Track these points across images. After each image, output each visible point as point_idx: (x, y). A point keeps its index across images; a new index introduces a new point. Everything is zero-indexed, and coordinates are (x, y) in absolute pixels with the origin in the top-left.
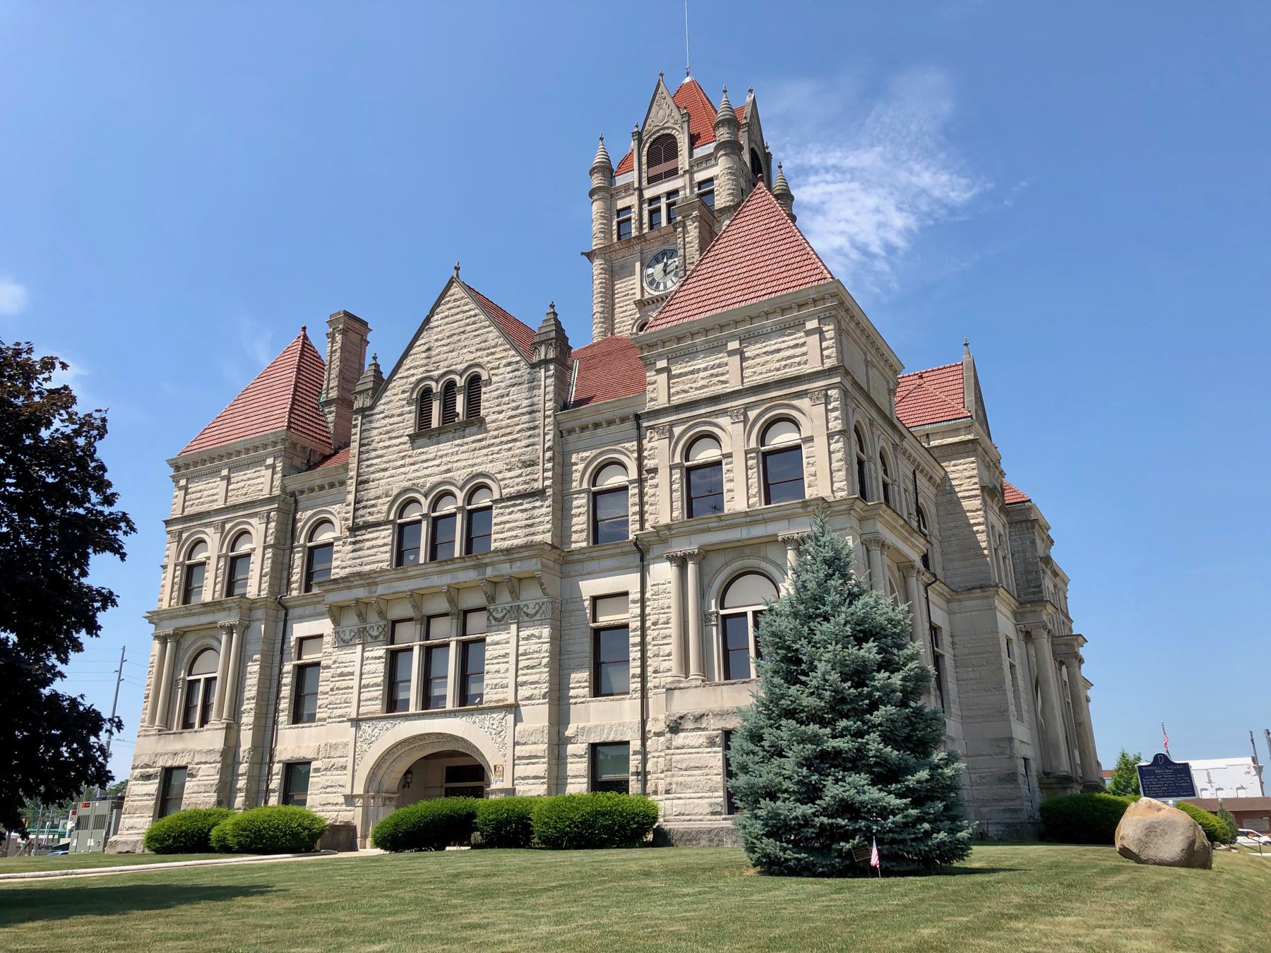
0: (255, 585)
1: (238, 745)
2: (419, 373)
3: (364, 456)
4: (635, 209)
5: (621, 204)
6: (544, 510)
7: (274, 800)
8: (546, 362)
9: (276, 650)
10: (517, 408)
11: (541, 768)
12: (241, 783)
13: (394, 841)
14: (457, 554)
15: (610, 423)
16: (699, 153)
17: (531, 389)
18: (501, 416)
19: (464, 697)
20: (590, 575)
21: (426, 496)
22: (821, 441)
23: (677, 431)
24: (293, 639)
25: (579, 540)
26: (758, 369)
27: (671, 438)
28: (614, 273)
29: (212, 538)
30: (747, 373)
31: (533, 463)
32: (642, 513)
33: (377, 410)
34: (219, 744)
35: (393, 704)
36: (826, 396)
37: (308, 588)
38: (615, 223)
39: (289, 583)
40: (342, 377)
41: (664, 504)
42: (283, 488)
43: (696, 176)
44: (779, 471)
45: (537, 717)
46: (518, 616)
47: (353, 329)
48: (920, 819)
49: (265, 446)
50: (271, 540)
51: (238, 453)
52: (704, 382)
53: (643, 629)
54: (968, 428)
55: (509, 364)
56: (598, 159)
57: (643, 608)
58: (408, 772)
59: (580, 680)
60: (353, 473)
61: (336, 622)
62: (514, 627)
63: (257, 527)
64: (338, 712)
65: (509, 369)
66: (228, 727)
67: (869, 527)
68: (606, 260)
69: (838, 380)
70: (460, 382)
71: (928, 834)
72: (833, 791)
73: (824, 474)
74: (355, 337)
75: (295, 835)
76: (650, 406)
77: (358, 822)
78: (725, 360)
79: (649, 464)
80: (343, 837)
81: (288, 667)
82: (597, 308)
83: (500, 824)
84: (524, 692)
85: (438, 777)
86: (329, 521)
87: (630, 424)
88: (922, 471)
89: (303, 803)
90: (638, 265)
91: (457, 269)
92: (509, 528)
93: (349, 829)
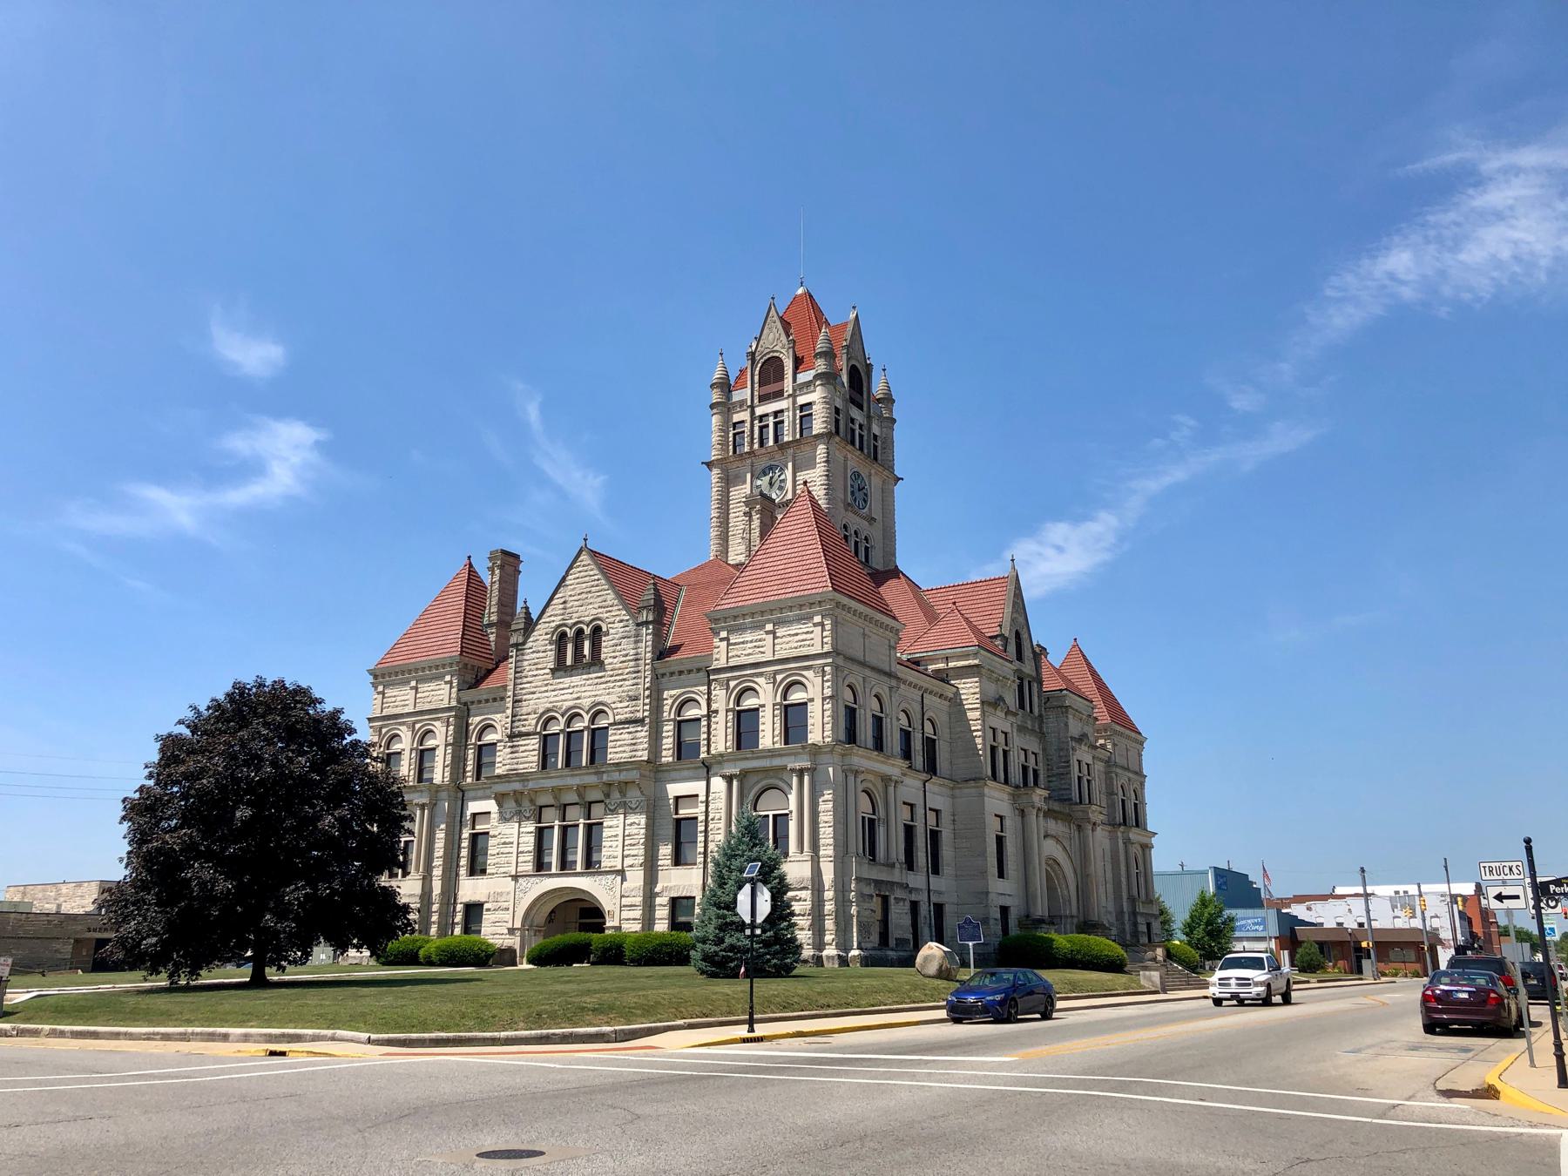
0: (440, 773)
2: (557, 621)
4: (748, 424)
5: (736, 418)
7: (458, 930)
8: (646, 623)
9: (457, 820)
11: (638, 913)
12: (435, 918)
13: (539, 959)
17: (636, 642)
19: (589, 863)
20: (674, 781)
22: (818, 702)
23: (732, 684)
25: (667, 756)
28: (728, 481)
29: (405, 734)
31: (636, 699)
32: (709, 740)
34: (418, 891)
35: (540, 866)
40: (501, 604)
41: (721, 739)
42: (459, 701)
45: (636, 878)
46: (628, 809)
47: (509, 562)
49: (444, 666)
50: (451, 740)
53: (706, 821)
54: (976, 655)
56: (718, 375)
58: (553, 911)
59: (666, 851)
61: (500, 805)
63: (439, 728)
66: (424, 878)
67: (847, 760)
70: (587, 631)
72: (728, 941)
73: (820, 727)
74: (509, 569)
75: (477, 956)
76: (715, 665)
77: (517, 947)
80: (506, 957)
81: (466, 834)
82: (714, 514)
83: (606, 950)
84: (628, 861)
85: (574, 915)
87: (702, 674)
92: (625, 747)
93: (511, 951)
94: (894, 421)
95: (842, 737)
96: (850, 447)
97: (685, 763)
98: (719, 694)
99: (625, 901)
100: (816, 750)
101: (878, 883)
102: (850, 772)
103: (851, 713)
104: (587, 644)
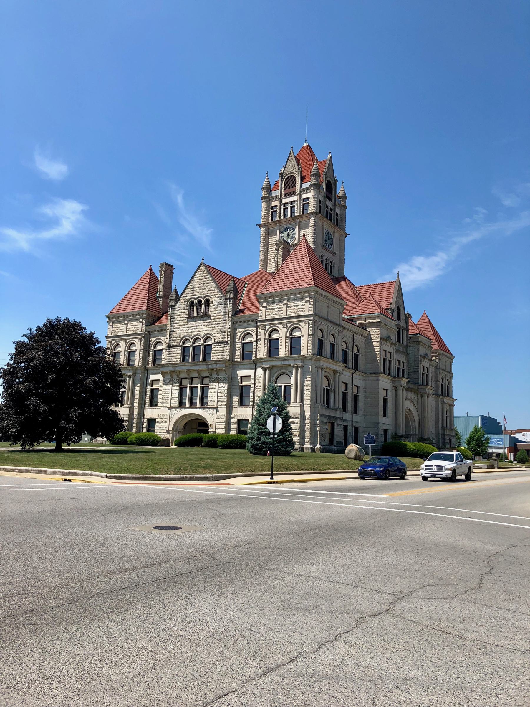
0: (137, 362)
1: (133, 413)
2: (190, 296)
3: (172, 322)
4: (278, 207)
5: (273, 204)
6: (227, 348)
7: (144, 430)
8: (230, 299)
9: (145, 383)
10: (220, 313)
11: (223, 426)
12: (135, 425)
13: (180, 444)
14: (201, 360)
15: (249, 321)
16: (305, 186)
17: (225, 307)
18: (215, 315)
21: (192, 339)
22: (306, 337)
23: (267, 327)
24: (150, 380)
25: (238, 358)
26: (291, 311)
27: (265, 329)
28: (269, 234)
29: (122, 344)
30: (288, 312)
31: (224, 332)
33: (176, 307)
34: (128, 413)
35: (181, 404)
36: (309, 323)
37: (154, 365)
38: (270, 212)
39: (148, 362)
40: (165, 287)
41: (262, 352)
43: (302, 196)
44: (294, 344)
45: (223, 411)
46: (220, 381)
47: (168, 269)
48: (279, 446)
49: (139, 315)
51: (130, 316)
52: (276, 313)
54: (379, 317)
55: (218, 297)
56: (265, 183)
57: (255, 381)
58: (186, 424)
59: (236, 399)
60: (168, 328)
61: (163, 377)
62: (217, 384)
63: (137, 342)
64: (164, 405)
65: (218, 299)
66: (130, 408)
67: (318, 363)
68: (266, 228)
69: (312, 318)
70: (203, 301)
71: (280, 449)
72: (262, 439)
73: (306, 348)
75: (153, 441)
76: (260, 318)
77: (170, 438)
78: (283, 306)
79: (259, 337)
80: (166, 442)
81: (149, 389)
82: (262, 249)
83: (209, 441)
85: (195, 426)
86: (161, 342)
87: (254, 322)
88: (357, 334)
89: (154, 431)
90: (278, 231)
91: (203, 259)
92: (219, 353)
93: (168, 440)
94: (346, 207)
95: (316, 352)
96: (325, 219)
97: (245, 361)
98: (261, 331)
99: (218, 420)
100: (304, 358)
101: (329, 417)
102: (319, 368)
103: (321, 342)
104: (203, 307)
